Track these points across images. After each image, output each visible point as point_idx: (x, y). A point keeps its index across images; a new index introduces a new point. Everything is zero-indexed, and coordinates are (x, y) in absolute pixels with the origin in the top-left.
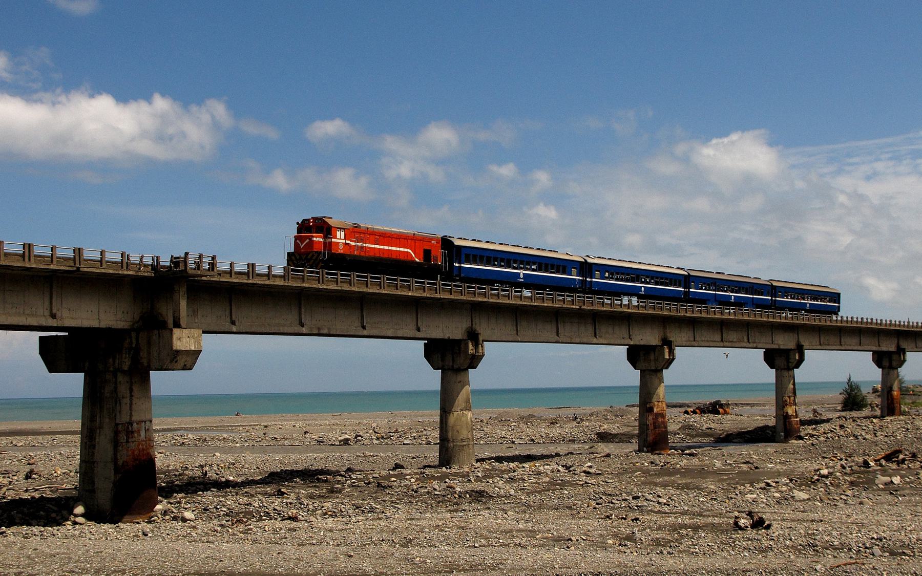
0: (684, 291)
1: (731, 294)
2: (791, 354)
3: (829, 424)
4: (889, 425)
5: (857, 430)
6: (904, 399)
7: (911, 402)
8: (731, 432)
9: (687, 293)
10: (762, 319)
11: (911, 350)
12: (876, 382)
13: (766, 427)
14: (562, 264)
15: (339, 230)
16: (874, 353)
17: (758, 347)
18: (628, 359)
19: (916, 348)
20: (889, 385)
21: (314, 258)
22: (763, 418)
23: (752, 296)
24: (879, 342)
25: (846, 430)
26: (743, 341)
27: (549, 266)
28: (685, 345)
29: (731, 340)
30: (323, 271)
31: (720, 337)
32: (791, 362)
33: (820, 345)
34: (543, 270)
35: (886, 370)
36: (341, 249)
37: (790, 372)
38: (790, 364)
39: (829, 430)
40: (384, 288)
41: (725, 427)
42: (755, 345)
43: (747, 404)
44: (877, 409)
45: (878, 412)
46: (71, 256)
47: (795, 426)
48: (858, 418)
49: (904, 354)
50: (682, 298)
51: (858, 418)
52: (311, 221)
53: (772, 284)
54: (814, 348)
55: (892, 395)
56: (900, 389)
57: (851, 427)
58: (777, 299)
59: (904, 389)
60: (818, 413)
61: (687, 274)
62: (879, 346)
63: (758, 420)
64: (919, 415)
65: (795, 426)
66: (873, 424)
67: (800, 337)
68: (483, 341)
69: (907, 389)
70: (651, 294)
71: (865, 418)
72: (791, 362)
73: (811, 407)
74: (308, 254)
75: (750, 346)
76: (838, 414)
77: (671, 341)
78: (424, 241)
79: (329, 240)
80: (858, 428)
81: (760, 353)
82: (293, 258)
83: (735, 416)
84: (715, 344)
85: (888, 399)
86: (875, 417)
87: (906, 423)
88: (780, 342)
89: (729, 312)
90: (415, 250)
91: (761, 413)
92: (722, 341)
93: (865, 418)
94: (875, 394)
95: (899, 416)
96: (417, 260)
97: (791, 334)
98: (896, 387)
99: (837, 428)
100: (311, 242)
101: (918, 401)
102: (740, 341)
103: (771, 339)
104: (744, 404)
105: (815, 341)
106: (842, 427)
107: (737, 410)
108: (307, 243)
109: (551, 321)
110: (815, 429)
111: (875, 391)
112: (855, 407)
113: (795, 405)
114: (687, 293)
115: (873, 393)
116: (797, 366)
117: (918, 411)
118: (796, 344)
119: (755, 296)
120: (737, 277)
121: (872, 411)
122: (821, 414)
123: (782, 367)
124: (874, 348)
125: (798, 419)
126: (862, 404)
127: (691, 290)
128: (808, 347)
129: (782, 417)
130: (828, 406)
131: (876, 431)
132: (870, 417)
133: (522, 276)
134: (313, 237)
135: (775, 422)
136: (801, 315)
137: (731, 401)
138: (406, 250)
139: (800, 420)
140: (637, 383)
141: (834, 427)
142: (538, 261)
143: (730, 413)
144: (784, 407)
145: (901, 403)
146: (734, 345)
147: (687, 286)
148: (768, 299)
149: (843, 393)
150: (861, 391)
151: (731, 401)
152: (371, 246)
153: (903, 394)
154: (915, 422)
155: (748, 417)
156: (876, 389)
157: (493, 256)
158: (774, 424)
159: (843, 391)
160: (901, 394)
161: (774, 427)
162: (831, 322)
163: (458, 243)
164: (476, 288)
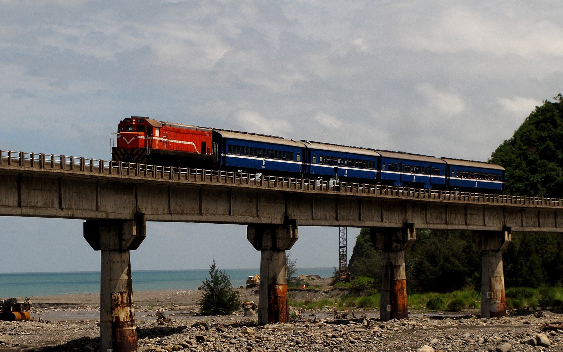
0: (377, 172)
1: (413, 174)
2: (126, 226)
3: (181, 335)
4: (271, 337)
5: (223, 344)
6: (293, 296)
7: (304, 301)
8: (31, 348)
9: (379, 174)
10: (82, 173)
11: (304, 222)
12: (253, 271)
13: (86, 340)
14: (286, 151)
15: (156, 129)
16: (251, 226)
17: (75, 216)
18: (84, 236)
19: (313, 219)
20: (271, 275)
21: (140, 153)
22: (82, 326)
23: (429, 176)
24: (257, 211)
25: (206, 345)
26: (53, 207)
27: (282, 153)
28: (317, 224)
29: (33, 204)
30: (249, 174)
31: (16, 198)
32: (124, 240)
33: (170, 213)
34: (266, 156)
35: (267, 253)
36: (157, 146)
37: (124, 256)
38: (124, 243)
39: (180, 344)
40: (121, 174)
41: (22, 341)
42: (70, 213)
43: (57, 304)
44: (254, 312)
45: (255, 317)
46: (58, 162)
47: (130, 338)
48: (225, 326)
49: (295, 228)
50: (375, 180)
51: (225, 326)
52: (134, 120)
53: (446, 163)
54: (161, 217)
55: (275, 291)
56: (288, 281)
57: (214, 339)
58: (451, 178)
59: (294, 281)
60: (165, 318)
61: (305, 147)
62: (258, 216)
63: (72, 329)
64: (314, 322)
65: (130, 338)
66: (246, 335)
67: (139, 201)
68: (147, 221)
69: (299, 282)
70: (357, 177)
71: (235, 326)
72: (124, 240)
73: (154, 308)
74: (133, 150)
75: (63, 214)
76: (195, 320)
77: (295, 220)
78: (202, 135)
79: (149, 138)
80: (225, 342)
81: (78, 225)
82: (119, 152)
83: (37, 324)
84: (8, 211)
85: (269, 298)
86: (250, 325)
87: (296, 334)
88: (109, 209)
89: (403, 192)
90: (197, 142)
91: (80, 318)
92: (19, 206)
93: (235, 326)
94: (250, 290)
95: (286, 322)
96: (197, 152)
97: (126, 197)
98: (281, 279)
99: (193, 341)
100: (137, 140)
101: (313, 300)
102: (47, 206)
103: (95, 203)
104: (53, 304)
105: (162, 207)
106: (200, 339)
107: (41, 313)
108: (133, 140)
109: (146, 197)
110: (159, 343)
111: (251, 284)
112: (220, 309)
113: (130, 305)
114: (379, 174)
115: (248, 287)
116: (135, 245)
117: (313, 316)
118: (133, 211)
119: (432, 176)
120: (414, 156)
121: (245, 315)
122: (170, 320)
123: (111, 248)
124: (250, 220)
125: (134, 328)
126: (232, 305)
127: (382, 171)
128: (151, 217)
129: (109, 324)
130: (180, 307)
131: (251, 345)
132: (243, 325)
133: (264, 164)
134: (138, 135)
135: (99, 332)
136: (238, 175)
137: (33, 299)
138: (189, 143)
139: (138, 329)
140: (97, 268)
141: (188, 340)
142: (275, 149)
143: (31, 318)
144: (113, 309)
145: (289, 303)
146: (38, 212)
147: (448, 174)
148: (443, 178)
149: (203, 288)
150: (230, 285)
151: (33, 299)
152: (172, 141)
153: (291, 290)
154: (309, 332)
155: (58, 324)
156: (253, 281)
157: (290, 151)
158: (99, 336)
159: (202, 284)
160: (288, 290)
161: (97, 340)
162: (186, 179)
163: (225, 135)
164: (146, 167)
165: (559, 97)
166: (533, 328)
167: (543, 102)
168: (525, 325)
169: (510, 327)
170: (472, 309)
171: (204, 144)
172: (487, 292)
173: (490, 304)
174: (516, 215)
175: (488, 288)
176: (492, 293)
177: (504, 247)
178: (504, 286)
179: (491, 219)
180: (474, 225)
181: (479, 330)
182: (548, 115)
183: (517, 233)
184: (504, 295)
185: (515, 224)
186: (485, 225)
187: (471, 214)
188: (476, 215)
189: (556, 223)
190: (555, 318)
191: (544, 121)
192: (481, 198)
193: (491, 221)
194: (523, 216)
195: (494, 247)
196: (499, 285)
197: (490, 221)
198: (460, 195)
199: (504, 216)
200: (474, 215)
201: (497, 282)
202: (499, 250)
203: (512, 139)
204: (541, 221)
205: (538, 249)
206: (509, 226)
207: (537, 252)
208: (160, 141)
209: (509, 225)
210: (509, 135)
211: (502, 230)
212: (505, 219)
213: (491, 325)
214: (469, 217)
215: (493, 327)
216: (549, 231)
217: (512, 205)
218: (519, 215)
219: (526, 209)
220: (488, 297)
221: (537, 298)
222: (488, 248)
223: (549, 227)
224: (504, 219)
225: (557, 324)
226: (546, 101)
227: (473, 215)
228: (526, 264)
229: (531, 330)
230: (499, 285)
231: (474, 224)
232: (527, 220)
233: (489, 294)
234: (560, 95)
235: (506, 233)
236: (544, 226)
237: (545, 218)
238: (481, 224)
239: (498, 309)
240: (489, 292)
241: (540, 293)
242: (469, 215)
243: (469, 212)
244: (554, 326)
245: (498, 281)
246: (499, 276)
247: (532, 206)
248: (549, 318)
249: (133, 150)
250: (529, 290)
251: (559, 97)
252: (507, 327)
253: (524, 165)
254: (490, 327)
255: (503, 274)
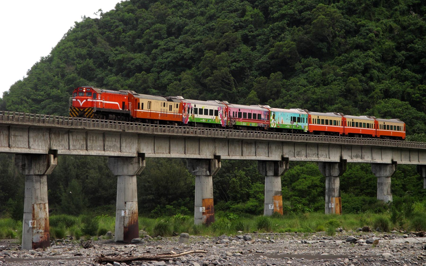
82: (74, 110)
165: (100, 12)
166: (87, 260)
167: (82, 18)
168: (77, 256)
169: (61, 259)
170: (10, 239)
171: (124, 103)
172: (30, 220)
173: (33, 234)
174: (63, 137)
175: (31, 216)
176: (35, 221)
177: (49, 171)
178: (48, 214)
179: (36, 141)
180: (18, 148)
181: (28, 263)
182: (89, 31)
183: (64, 156)
184: (48, 223)
185: (62, 146)
186: (29, 148)
187: (15, 136)
188: (20, 137)
189: (104, 146)
190: (105, 248)
191: (84, 37)
192: (26, 118)
193: (37, 143)
194: (70, 139)
195: (38, 172)
196: (42, 213)
197: (35, 143)
198: (4, 115)
199: (50, 138)
200: (18, 137)
201: (41, 209)
202: (44, 175)
203: (49, 56)
204: (89, 144)
205: (78, 174)
206: (55, 149)
207: (77, 177)
208: (101, 102)
209: (55, 148)
210: (46, 53)
211: (47, 153)
212: (51, 142)
213: (40, 257)
214: (13, 139)
215: (43, 259)
216: (97, 155)
217: (59, 126)
218: (66, 137)
219: (73, 130)
220: (30, 226)
221: (79, 226)
222: (32, 173)
223: (97, 150)
224: (50, 141)
225: (113, 256)
226: (85, 16)
227: (17, 136)
228: (65, 190)
229: (85, 263)
230: (42, 213)
231: (18, 146)
232: (74, 142)
233: (31, 223)
234: (100, 10)
235: (52, 156)
236: (92, 149)
237: (93, 140)
238: (25, 147)
239: (41, 239)
240: (33, 220)
241: (83, 221)
242: (12, 137)
243: (12, 133)
244: (110, 257)
245: (42, 208)
246: (43, 203)
247: (80, 127)
248: (99, 249)
249: (85, 108)
250: (72, 218)
251: (100, 12)
252: (58, 259)
253: (62, 85)
254: (39, 259)
255: (47, 202)
